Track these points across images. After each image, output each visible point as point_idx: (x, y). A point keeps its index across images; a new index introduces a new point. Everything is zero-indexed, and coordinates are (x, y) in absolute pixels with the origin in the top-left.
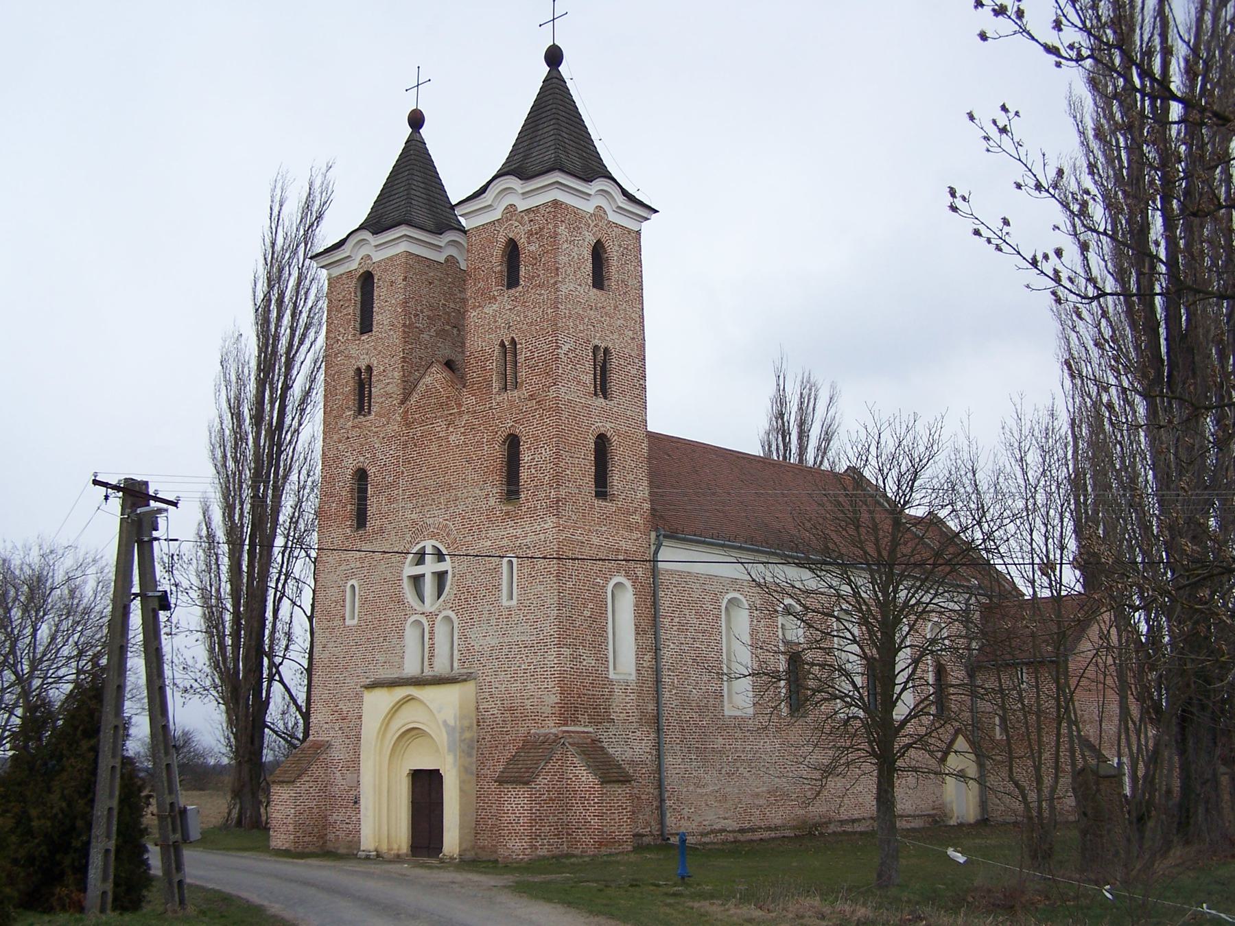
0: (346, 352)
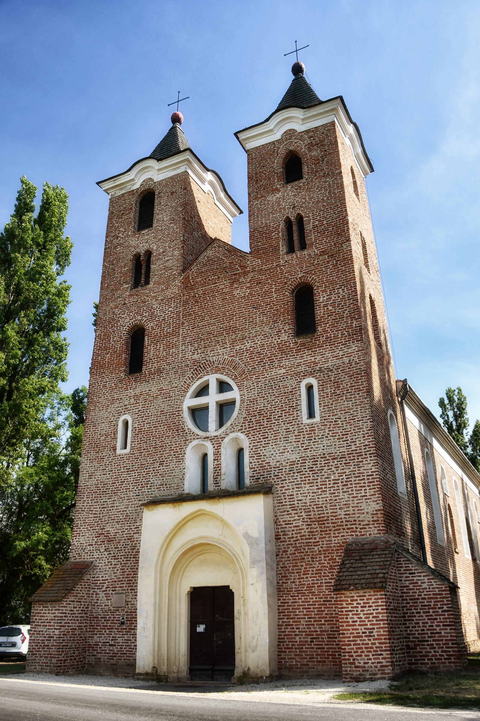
0: (126, 244)
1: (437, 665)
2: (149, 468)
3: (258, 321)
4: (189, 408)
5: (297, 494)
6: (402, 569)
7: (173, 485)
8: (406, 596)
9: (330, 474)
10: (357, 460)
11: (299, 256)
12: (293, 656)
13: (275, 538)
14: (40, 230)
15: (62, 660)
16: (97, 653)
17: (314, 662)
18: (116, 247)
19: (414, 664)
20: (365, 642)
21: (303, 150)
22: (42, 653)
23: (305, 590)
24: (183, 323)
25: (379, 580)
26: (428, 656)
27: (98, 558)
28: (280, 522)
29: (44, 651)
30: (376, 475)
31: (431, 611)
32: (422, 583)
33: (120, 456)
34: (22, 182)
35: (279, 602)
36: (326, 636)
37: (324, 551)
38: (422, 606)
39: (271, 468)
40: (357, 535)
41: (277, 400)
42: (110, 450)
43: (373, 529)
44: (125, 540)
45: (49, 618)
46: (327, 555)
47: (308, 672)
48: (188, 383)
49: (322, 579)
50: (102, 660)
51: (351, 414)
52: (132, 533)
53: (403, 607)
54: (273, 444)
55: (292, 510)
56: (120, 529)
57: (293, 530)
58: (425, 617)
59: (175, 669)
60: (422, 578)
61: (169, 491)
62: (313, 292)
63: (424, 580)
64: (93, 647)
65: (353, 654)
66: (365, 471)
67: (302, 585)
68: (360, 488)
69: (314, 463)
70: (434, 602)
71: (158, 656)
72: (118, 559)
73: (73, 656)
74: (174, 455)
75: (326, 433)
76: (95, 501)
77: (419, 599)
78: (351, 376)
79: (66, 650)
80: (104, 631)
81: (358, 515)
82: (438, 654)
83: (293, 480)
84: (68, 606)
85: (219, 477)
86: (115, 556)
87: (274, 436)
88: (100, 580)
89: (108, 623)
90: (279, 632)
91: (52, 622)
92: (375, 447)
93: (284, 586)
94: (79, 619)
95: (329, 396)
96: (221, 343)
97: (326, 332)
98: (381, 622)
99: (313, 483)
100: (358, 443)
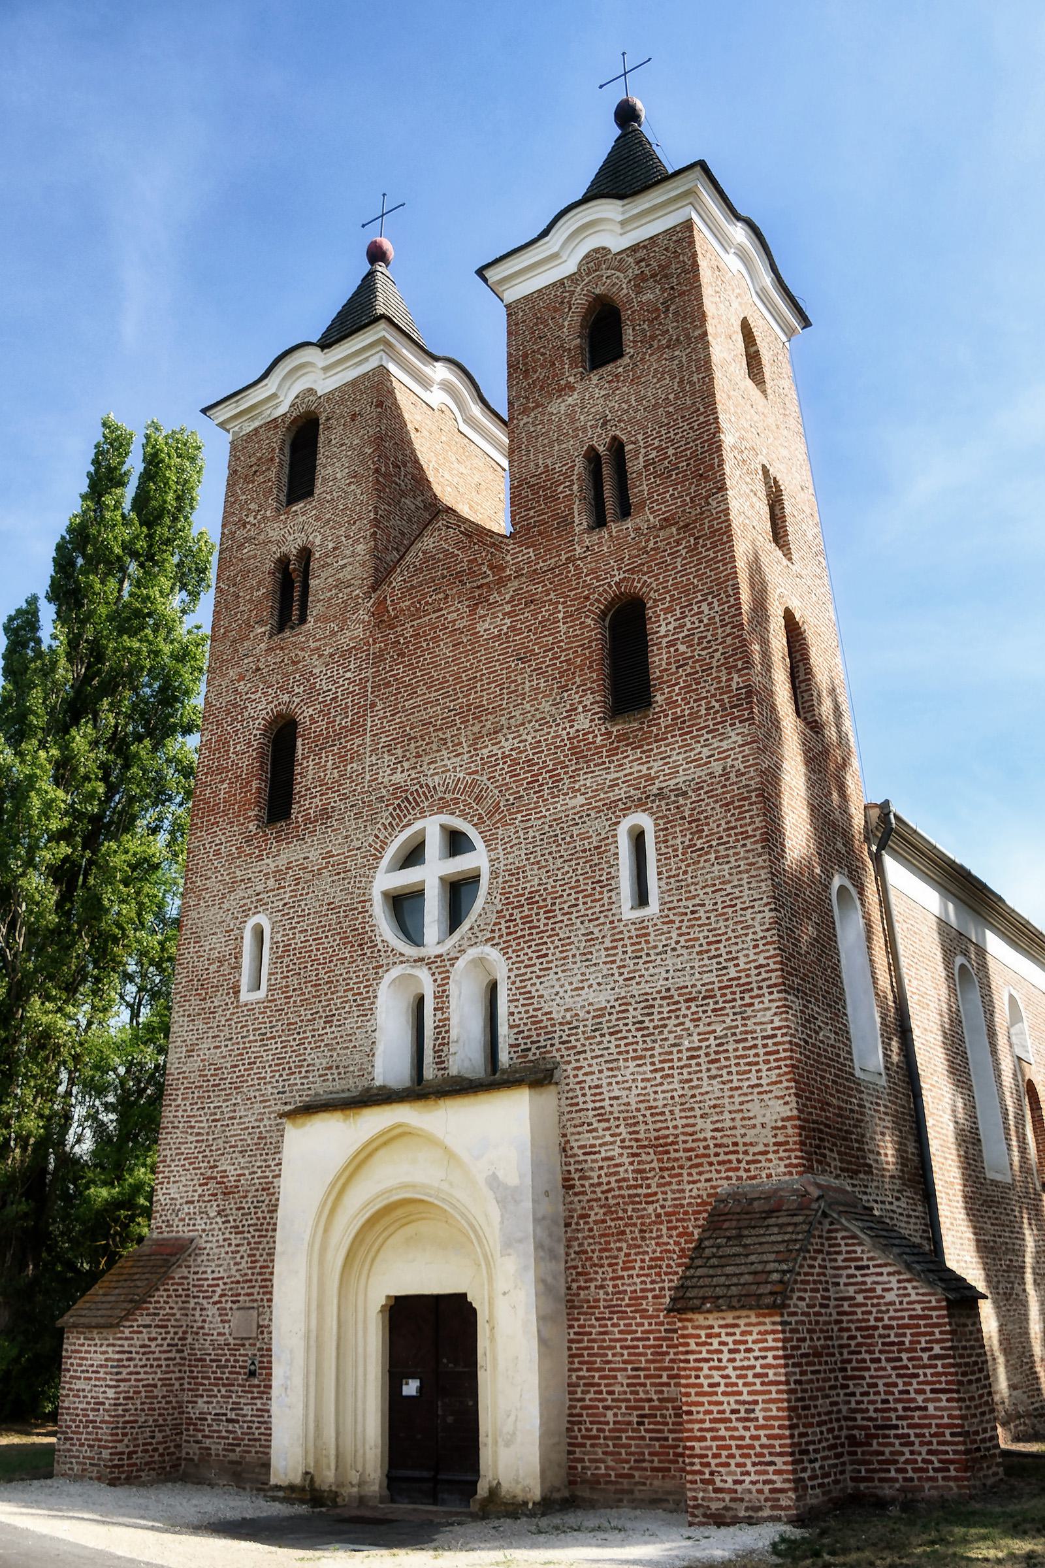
0: (262, 537)
1: (916, 1483)
2: (305, 1032)
3: (527, 689)
4: (385, 894)
5: (610, 1084)
6: (840, 1258)
7: (351, 1069)
8: (849, 1321)
9: (681, 1037)
10: (740, 1002)
11: (614, 534)
12: (601, 1456)
13: (564, 1187)
14: (141, 526)
15: (122, 1453)
16: (203, 1436)
17: (645, 1469)
18: (241, 547)
19: (864, 1479)
20: (736, 1434)
21: (625, 291)
22: (84, 1436)
23: (628, 1306)
24: (373, 705)
25: (769, 1288)
26: (896, 1462)
27: (204, 1231)
28: (572, 1148)
29: (87, 1433)
30: (783, 1035)
31: (904, 1356)
32: (884, 1290)
33: (246, 1005)
34: (104, 425)
35: (572, 1331)
36: (672, 1412)
37: (667, 1214)
38: (884, 1344)
39: (553, 1025)
40: (739, 1178)
41: (566, 869)
42: (228, 994)
43: (775, 1162)
44: (257, 1190)
45: (95, 1363)
46: (674, 1224)
47: (631, 1492)
48: (382, 837)
49: (664, 1281)
50: (213, 1452)
51: (727, 895)
52: (271, 1175)
53: (841, 1346)
54: (559, 970)
55: (599, 1121)
56: (247, 1168)
57: (601, 1168)
58: (890, 1372)
59: (354, 1477)
60: (885, 1278)
61: (344, 1082)
62: (644, 615)
63: (889, 1282)
64: (195, 1424)
65: (709, 1459)
66: (758, 1028)
67: (619, 1293)
68: (747, 1068)
69: (646, 1011)
70: (911, 1335)
71: (316, 1446)
72: (243, 1232)
73: (151, 1444)
74: (355, 1001)
75: (672, 941)
76: (199, 1105)
77: (876, 1328)
78: (727, 805)
79: (134, 1431)
80: (216, 1389)
81: (743, 1131)
82: (919, 1459)
83: (600, 1053)
84: (135, 1336)
85: (445, 1048)
86: (237, 1227)
87: (561, 952)
88: (207, 1279)
89: (224, 1373)
90: (571, 1400)
91: (102, 1370)
92: (782, 970)
93: (582, 1296)
94: (164, 1363)
95: (679, 853)
96: (450, 744)
97: (672, 703)
98: (773, 1388)
99: (644, 1057)
100: (742, 961)
